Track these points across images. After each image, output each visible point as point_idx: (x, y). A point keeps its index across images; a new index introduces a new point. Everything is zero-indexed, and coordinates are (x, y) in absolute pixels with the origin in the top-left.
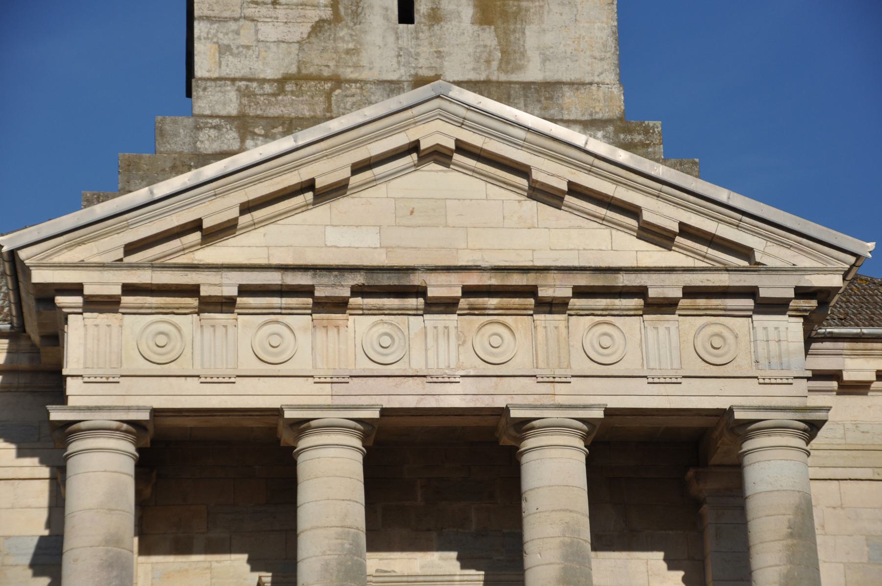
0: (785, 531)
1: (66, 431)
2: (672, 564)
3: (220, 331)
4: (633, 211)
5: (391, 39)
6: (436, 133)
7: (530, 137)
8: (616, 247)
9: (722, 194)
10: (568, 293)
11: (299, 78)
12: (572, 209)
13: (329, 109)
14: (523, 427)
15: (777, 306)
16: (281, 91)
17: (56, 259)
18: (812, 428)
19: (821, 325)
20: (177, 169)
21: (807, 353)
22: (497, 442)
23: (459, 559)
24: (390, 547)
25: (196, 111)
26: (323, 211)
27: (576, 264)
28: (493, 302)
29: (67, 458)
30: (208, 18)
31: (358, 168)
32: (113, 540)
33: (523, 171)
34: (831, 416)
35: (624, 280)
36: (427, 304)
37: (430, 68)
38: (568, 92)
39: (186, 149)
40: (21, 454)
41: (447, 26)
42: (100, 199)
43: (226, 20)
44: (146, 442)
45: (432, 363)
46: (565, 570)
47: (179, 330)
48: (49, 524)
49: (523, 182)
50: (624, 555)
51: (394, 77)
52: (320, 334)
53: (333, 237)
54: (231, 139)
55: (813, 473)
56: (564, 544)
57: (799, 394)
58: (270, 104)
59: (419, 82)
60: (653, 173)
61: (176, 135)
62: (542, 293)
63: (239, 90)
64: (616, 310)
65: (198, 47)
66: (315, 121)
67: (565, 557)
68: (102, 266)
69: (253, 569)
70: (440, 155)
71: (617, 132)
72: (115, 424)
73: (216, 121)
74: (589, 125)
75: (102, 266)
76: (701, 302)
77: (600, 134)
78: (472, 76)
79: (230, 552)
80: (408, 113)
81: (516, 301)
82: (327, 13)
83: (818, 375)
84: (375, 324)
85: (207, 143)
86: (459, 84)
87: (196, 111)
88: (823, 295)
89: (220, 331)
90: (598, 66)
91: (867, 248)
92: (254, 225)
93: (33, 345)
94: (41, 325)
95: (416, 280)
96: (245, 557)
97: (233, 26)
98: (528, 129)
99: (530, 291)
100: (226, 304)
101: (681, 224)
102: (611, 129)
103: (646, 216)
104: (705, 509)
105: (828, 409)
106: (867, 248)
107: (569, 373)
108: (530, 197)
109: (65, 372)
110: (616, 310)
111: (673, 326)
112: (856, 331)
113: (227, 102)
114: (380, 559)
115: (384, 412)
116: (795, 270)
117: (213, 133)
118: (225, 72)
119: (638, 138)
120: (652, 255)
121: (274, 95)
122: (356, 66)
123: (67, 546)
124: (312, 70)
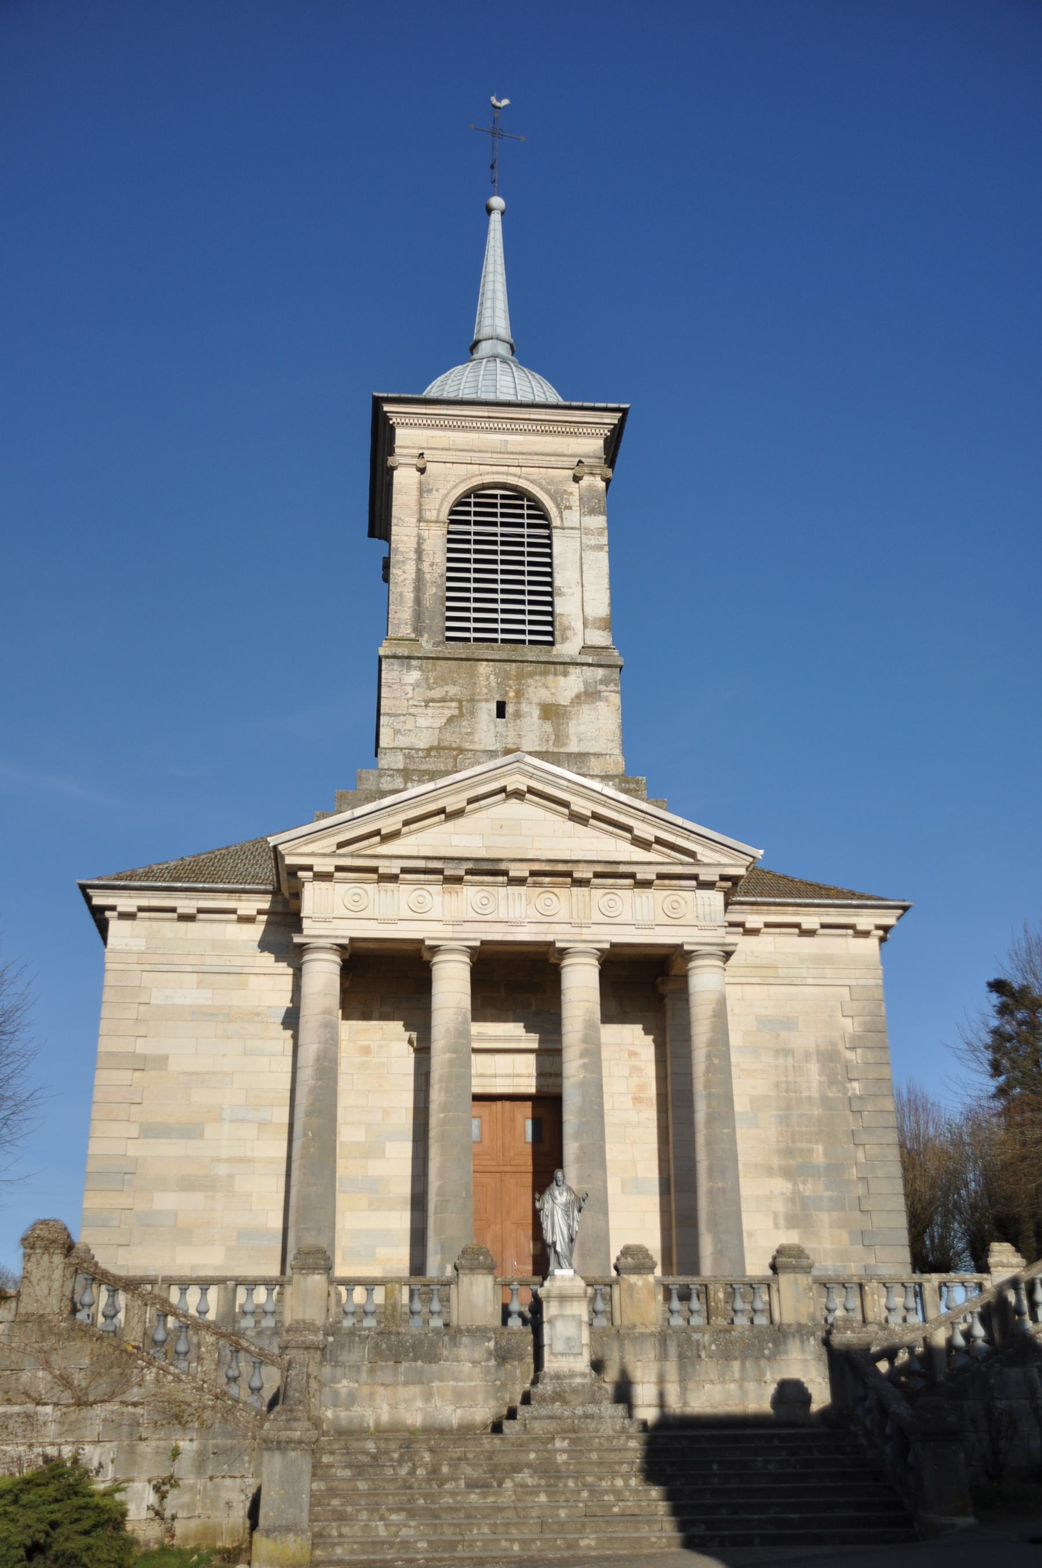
0: (710, 1013)
1: (301, 949)
2: (647, 1032)
3: (390, 894)
4: (629, 829)
5: (492, 727)
6: (519, 782)
7: (570, 785)
8: (617, 849)
9: (679, 821)
10: (591, 875)
11: (438, 748)
12: (594, 827)
13: (455, 766)
14: (563, 952)
15: (709, 885)
16: (428, 755)
17: (299, 851)
18: (728, 955)
19: (734, 895)
20: (369, 799)
21: (726, 911)
22: (547, 960)
23: (525, 1027)
24: (485, 1020)
25: (380, 766)
26: (451, 825)
27: (595, 859)
28: (547, 879)
29: (302, 964)
30: (388, 714)
31: (471, 801)
32: (328, 1012)
33: (565, 804)
34: (738, 948)
35: (622, 869)
36: (636, 883)
37: (514, 744)
38: (593, 759)
39: (373, 788)
40: (277, 961)
42: (325, 816)
43: (399, 715)
44: (347, 956)
45: (511, 915)
46: (586, 1035)
47: (366, 892)
48: (292, 1001)
49: (566, 811)
50: (619, 1026)
51: (493, 748)
52: (447, 896)
53: (455, 840)
54: (399, 782)
55: (727, 980)
56: (585, 1020)
57: (721, 936)
58: (422, 762)
59: (508, 752)
60: (640, 807)
61: (368, 780)
62: (575, 875)
63: (404, 754)
64: (408, 447)
65: (382, 730)
66: (447, 773)
67: (586, 1028)
68: (324, 855)
69: (406, 1030)
70: (518, 795)
71: (620, 783)
72: (329, 946)
73: (391, 772)
74: (605, 778)
75: (324, 855)
76: (667, 882)
77: (611, 783)
78: (538, 749)
79: (393, 1020)
80: (501, 770)
81: (561, 879)
82: (456, 712)
83: (732, 925)
84: (479, 891)
85: (386, 784)
86: (530, 753)
87: (380, 766)
88: (734, 880)
89: (390, 894)
90: (610, 745)
91: (759, 853)
92: (410, 833)
93: (285, 898)
94: (289, 888)
95: (503, 866)
96: (402, 1023)
97: (402, 718)
98: (569, 781)
99: (569, 874)
100: (393, 878)
101: (656, 837)
102: (617, 780)
103: (636, 832)
104: (667, 1000)
105: (736, 945)
106: (759, 853)
107: (591, 921)
108: (569, 819)
109: (302, 915)
110: (408, 447)
111: (650, 896)
112: (753, 899)
113: (398, 761)
115: (483, 942)
116: (719, 865)
117: (389, 779)
118: (397, 744)
119: (632, 786)
120: (639, 854)
121: (424, 758)
122: (472, 742)
123: (301, 1014)
124: (446, 744)
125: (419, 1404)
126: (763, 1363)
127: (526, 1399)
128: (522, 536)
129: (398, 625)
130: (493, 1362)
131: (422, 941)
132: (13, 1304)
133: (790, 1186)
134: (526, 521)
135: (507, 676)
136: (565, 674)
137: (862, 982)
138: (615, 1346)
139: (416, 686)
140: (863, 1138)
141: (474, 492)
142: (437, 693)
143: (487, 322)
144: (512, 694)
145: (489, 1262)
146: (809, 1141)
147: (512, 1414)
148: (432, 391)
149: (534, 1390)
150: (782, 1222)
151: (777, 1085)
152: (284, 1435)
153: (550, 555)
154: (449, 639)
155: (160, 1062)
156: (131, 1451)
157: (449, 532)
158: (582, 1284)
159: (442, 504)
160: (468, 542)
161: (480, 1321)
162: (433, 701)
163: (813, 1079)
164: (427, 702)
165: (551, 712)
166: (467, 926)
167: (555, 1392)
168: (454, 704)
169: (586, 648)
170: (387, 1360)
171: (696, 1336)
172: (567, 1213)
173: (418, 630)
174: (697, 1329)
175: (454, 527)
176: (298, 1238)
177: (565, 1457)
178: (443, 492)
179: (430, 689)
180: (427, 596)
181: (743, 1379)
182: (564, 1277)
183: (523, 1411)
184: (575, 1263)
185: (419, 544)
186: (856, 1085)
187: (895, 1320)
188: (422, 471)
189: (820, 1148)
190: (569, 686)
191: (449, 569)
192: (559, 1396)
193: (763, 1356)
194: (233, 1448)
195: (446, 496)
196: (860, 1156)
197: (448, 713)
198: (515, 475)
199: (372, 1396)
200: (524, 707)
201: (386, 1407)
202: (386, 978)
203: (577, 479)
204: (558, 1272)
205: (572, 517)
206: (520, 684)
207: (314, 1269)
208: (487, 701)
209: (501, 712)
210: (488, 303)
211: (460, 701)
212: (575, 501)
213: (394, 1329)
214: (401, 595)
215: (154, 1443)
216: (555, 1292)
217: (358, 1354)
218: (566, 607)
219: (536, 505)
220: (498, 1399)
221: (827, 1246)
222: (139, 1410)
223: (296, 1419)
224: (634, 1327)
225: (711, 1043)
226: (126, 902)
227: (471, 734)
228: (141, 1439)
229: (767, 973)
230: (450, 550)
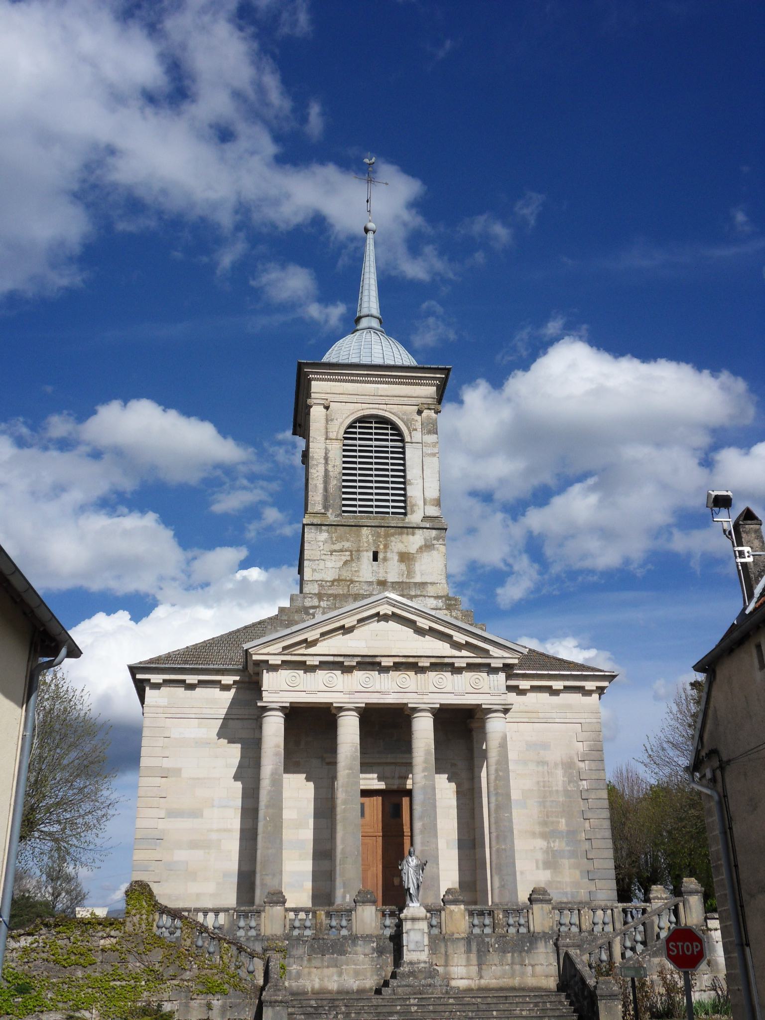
8: (442, 649)
11: (339, 580)
16: (333, 585)
17: (260, 652)
35: (447, 660)
41: (389, 563)
82: (349, 558)
90: (440, 577)
95: (378, 659)
120: (456, 653)
124: (343, 578)
125: (335, 978)
126: (524, 954)
127: (394, 975)
128: (387, 447)
129: (314, 505)
130: (375, 955)
131: (332, 704)
133: (545, 844)
134: (390, 437)
135: (379, 536)
137: (588, 720)
138: (443, 945)
139: (325, 542)
140: (588, 815)
141: (362, 420)
142: (337, 547)
143: (365, 305)
144: (382, 547)
145: (373, 899)
146: (557, 817)
147: (386, 984)
148: (330, 356)
149: (398, 971)
150: (541, 865)
151: (538, 783)
152: (273, 998)
154: (344, 512)
155: (177, 772)
156: (187, 1005)
157: (344, 445)
158: (425, 911)
160: (355, 451)
162: (335, 551)
163: (559, 779)
164: (332, 552)
165: (405, 558)
167: (409, 971)
168: (348, 553)
169: (426, 518)
170: (317, 954)
171: (486, 939)
172: (417, 873)
173: (326, 507)
174: (487, 935)
175: (347, 442)
177: (416, 1008)
178: (340, 420)
179: (334, 544)
181: (513, 963)
182: (414, 908)
183: (393, 983)
184: (420, 898)
185: (326, 454)
186: (584, 782)
187: (598, 929)
188: (327, 408)
189: (563, 820)
190: (415, 541)
191: (344, 468)
192: (412, 974)
193: (524, 950)
194: (239, 1004)
195: (342, 423)
196: (587, 824)
197: (344, 559)
199: (309, 973)
200: (389, 555)
201: (317, 980)
202: (311, 726)
203: (420, 412)
205: (417, 436)
206: (386, 540)
208: (367, 551)
209: (375, 559)
210: (366, 293)
211: (351, 551)
212: (418, 425)
213: (321, 936)
214: (316, 486)
215: (198, 1001)
216: (409, 916)
217: (300, 951)
218: (414, 492)
219: (395, 427)
220: (378, 975)
221: (567, 879)
223: (280, 990)
224: (453, 934)
225: (498, 763)
226: (156, 678)
228: (191, 999)
229: (533, 718)
230: (344, 456)
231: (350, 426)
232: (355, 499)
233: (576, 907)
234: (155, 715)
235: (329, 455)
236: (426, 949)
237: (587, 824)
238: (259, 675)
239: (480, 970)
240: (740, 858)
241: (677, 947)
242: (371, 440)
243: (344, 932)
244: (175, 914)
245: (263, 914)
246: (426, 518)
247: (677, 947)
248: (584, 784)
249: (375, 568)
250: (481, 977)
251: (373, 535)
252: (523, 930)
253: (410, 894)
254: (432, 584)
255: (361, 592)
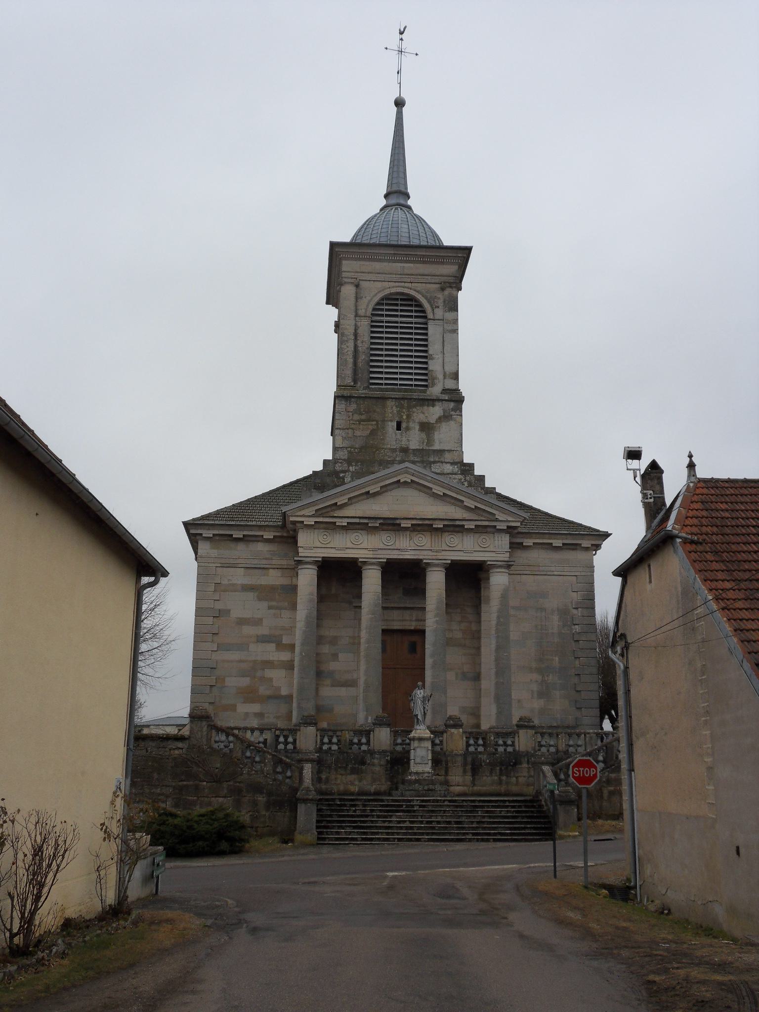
5: (394, 435)
26: (371, 501)
35: (458, 523)
95: (398, 522)
114: (631, 770)
125: (357, 783)
132: (187, 742)
133: (540, 677)
134: (414, 314)
135: (402, 407)
136: (433, 406)
141: (386, 298)
144: (405, 417)
150: (535, 695)
153: (426, 334)
159: (368, 306)
161: (384, 748)
162: (363, 421)
165: (426, 428)
166: (380, 552)
168: (374, 423)
173: (355, 381)
174: (480, 753)
176: (299, 707)
178: (368, 298)
180: (360, 360)
185: (356, 330)
188: (357, 286)
198: (408, 288)
200: (411, 425)
202: (339, 575)
204: (418, 727)
207: (310, 724)
208: (391, 421)
209: (399, 427)
212: (440, 303)
222: (242, 785)
227: (383, 439)
231: (378, 304)
232: (387, 350)
233: (552, 731)
234: (206, 565)
235: (359, 331)
236: (430, 762)
237: (577, 662)
238: (295, 531)
239: (474, 780)
240: (634, 711)
241: (579, 771)
242: (396, 316)
243: (364, 748)
244: (228, 731)
245: (298, 733)
246: (445, 391)
247: (579, 771)
248: (577, 628)
249: (399, 437)
250: (474, 785)
251: (397, 407)
252: (510, 749)
253: (418, 719)
254: (449, 451)
255: (386, 458)
